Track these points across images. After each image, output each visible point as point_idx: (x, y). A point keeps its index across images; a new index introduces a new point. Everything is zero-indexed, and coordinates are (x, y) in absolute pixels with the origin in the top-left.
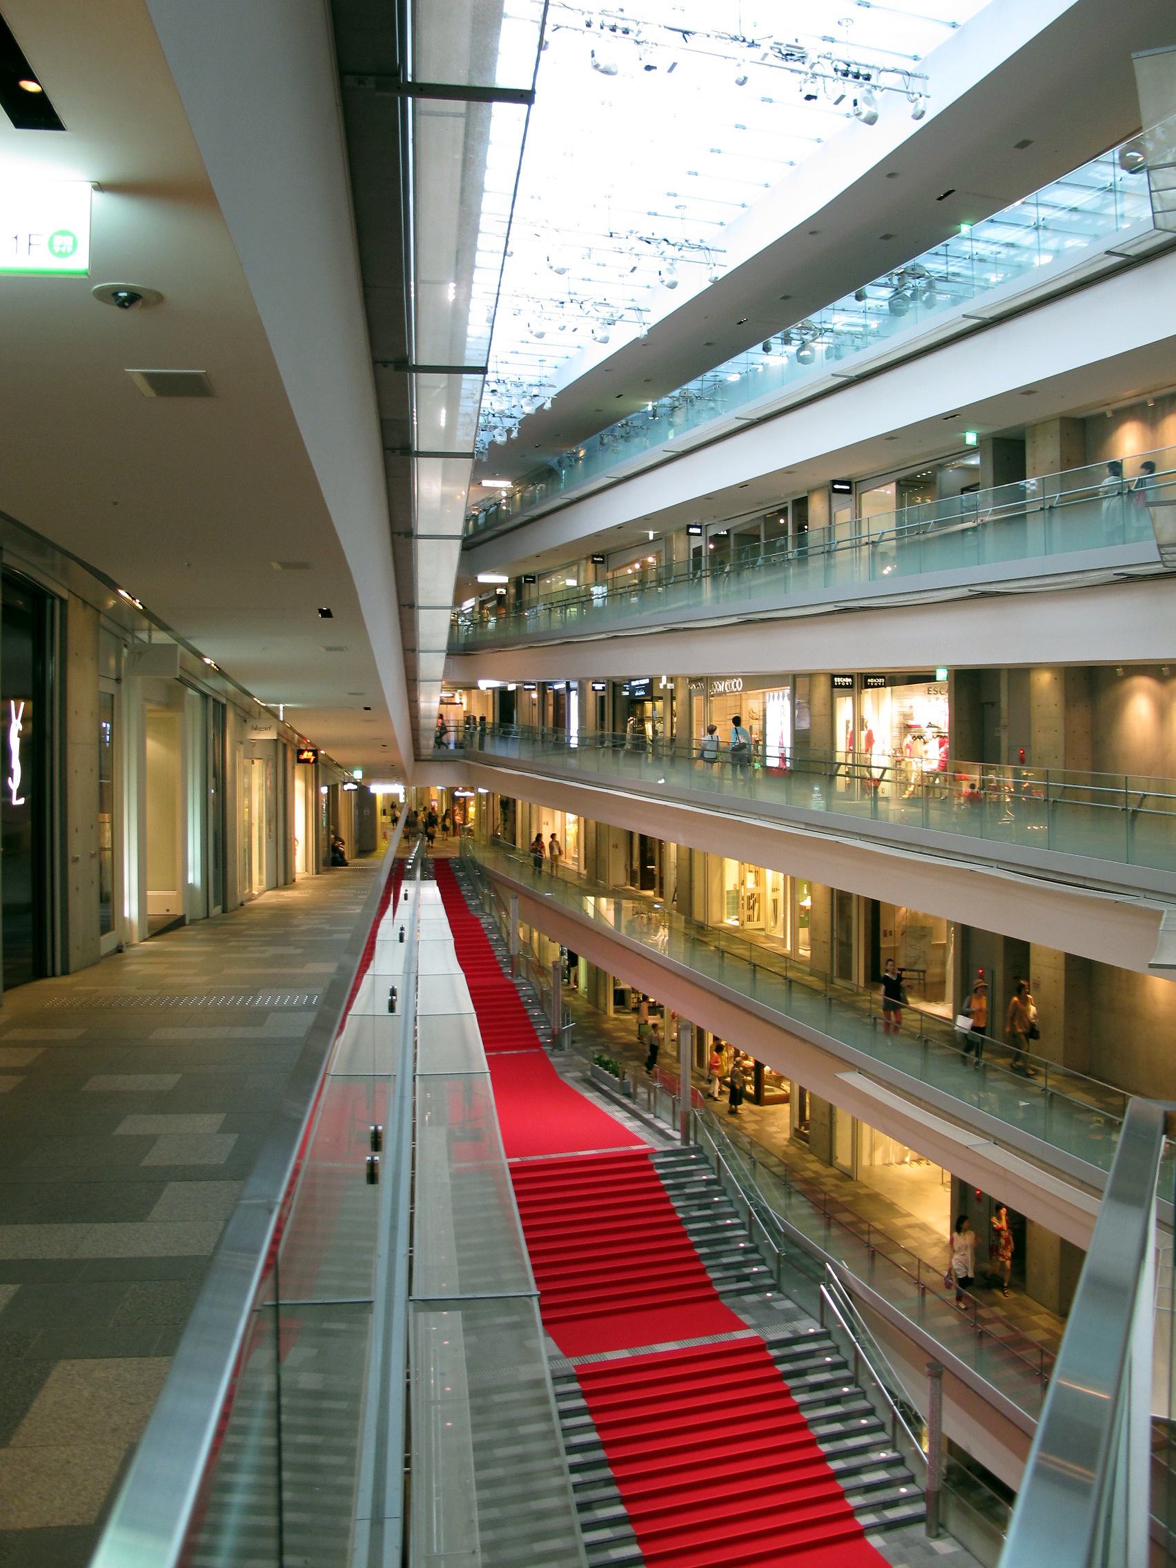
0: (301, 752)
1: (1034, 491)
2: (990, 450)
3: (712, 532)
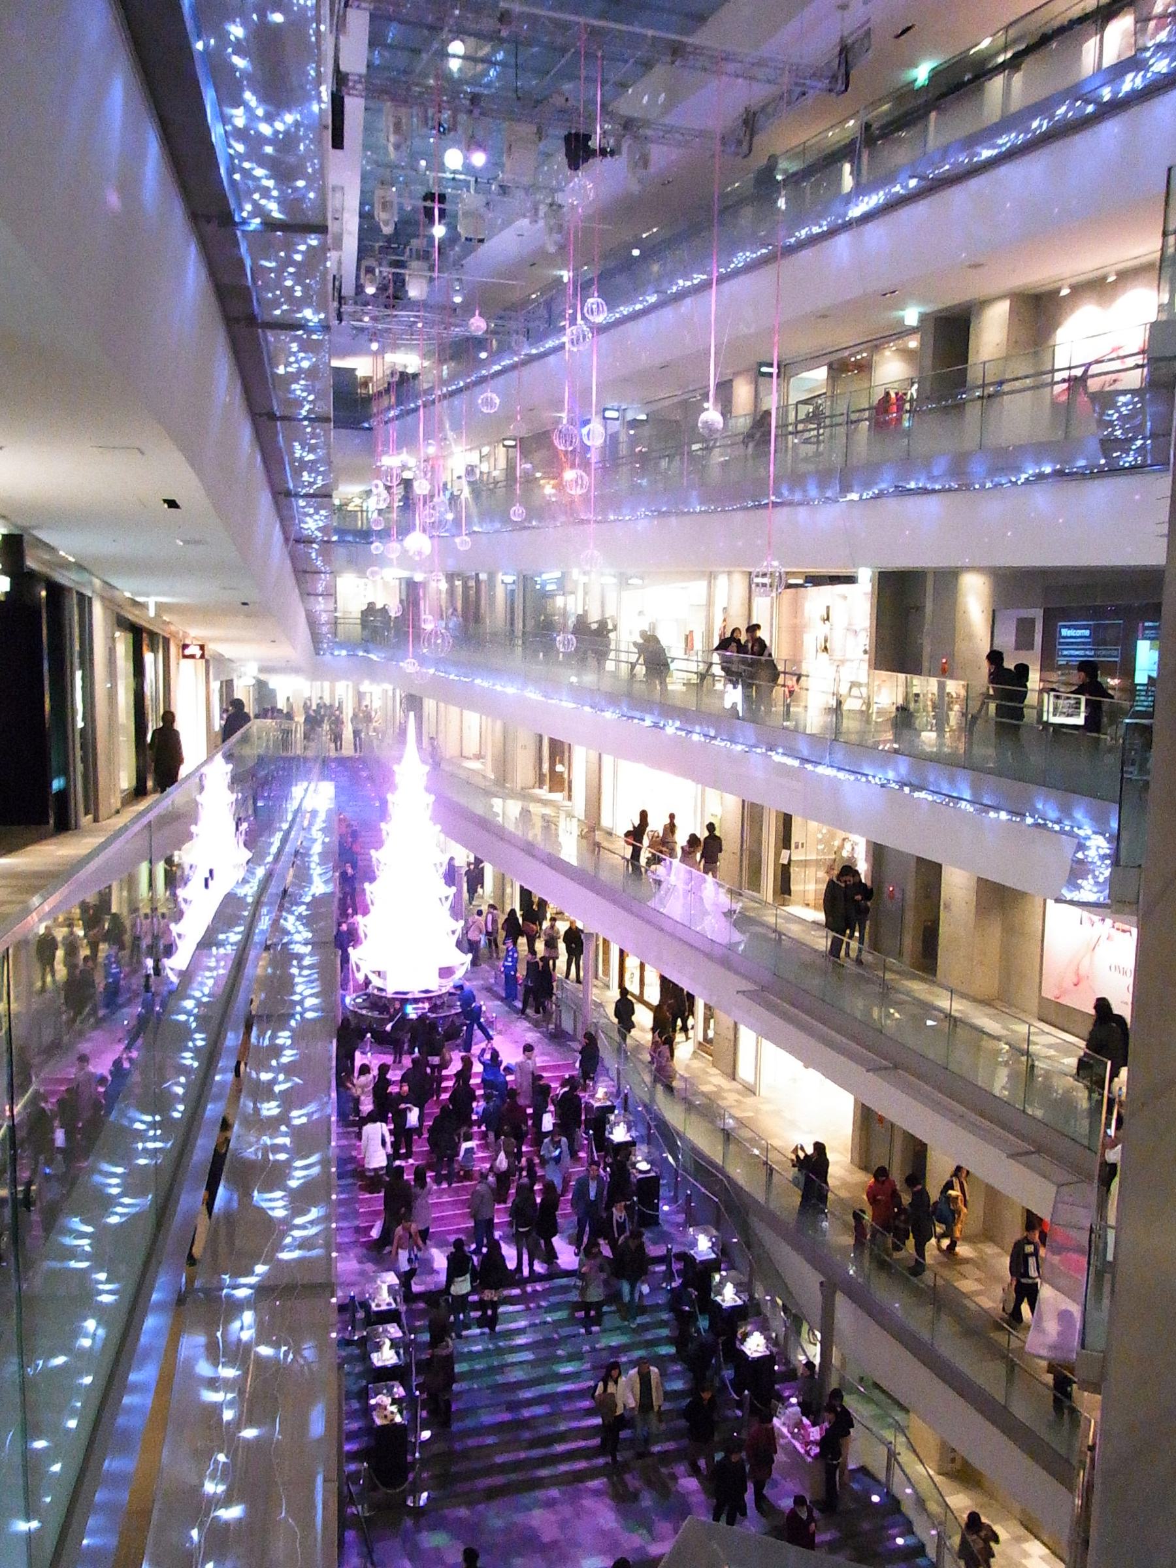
0: (185, 646)
1: (439, 1246)
2: (931, 329)
3: (630, 416)
